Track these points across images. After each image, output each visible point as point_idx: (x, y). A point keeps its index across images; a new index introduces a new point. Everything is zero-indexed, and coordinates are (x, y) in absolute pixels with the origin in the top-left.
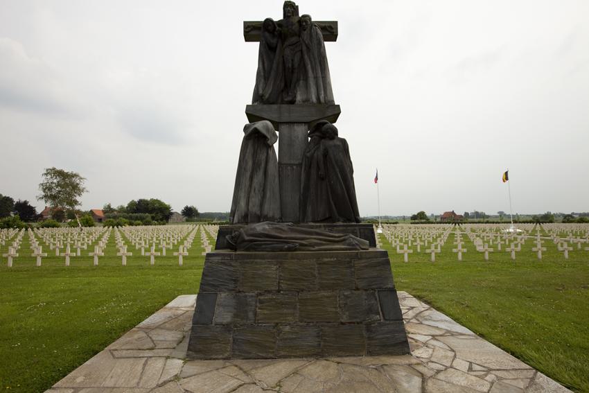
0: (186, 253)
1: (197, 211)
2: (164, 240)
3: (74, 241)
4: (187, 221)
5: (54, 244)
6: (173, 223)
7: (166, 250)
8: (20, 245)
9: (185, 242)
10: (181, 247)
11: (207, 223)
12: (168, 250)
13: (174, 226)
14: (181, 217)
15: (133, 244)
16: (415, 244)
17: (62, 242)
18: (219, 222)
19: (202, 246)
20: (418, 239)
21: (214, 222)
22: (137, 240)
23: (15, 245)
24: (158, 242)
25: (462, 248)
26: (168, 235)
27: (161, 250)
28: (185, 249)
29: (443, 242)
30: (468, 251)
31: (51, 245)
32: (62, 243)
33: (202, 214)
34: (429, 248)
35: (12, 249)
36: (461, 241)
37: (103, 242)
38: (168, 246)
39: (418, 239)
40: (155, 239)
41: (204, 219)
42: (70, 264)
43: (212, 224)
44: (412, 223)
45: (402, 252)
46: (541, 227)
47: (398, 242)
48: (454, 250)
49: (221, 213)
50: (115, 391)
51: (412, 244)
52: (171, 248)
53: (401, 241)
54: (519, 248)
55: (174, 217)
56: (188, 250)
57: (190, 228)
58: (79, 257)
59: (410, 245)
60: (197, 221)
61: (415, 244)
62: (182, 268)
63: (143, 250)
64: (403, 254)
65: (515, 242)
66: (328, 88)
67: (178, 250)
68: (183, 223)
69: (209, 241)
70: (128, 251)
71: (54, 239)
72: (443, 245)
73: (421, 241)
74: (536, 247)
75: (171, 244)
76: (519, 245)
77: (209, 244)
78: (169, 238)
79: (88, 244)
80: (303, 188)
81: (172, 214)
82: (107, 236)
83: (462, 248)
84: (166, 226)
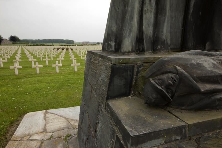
0: (63, 59)
1: (18, 38)
2: (51, 53)
3: (49, 53)
4: (13, 44)
5: (36, 53)
6: (4, 45)
8: (20, 55)
9: (62, 53)
10: (60, 56)
11: (25, 45)
12: (54, 57)
13: (5, 47)
14: (9, 41)
16: (44, 60)
17: (43, 53)
18: (33, 44)
19: (70, 55)
20: (47, 57)
21: (30, 44)
23: (19, 56)
24: (48, 54)
26: (2, 52)
27: (50, 58)
28: (62, 57)
30: (70, 65)
32: (43, 55)
33: (22, 40)
35: (18, 58)
37: (19, 55)
38: (54, 56)
39: (47, 57)
40: (46, 53)
41: (24, 43)
43: (29, 45)
44: (60, 45)
46: (22, 47)
47: (81, 54)
49: (32, 40)
52: (55, 56)
53: (83, 54)
55: (4, 41)
56: (63, 57)
57: (14, 47)
58: (52, 61)
59: (84, 53)
60: (19, 44)
61: (44, 60)
62: (18, 78)
65: (53, 54)
68: (11, 45)
69: (73, 53)
71: (34, 51)
73: (49, 58)
75: (55, 55)
77: (73, 54)
78: (4, 54)
79: (56, 55)
80: (194, 6)
81: (3, 40)
82: (20, 52)
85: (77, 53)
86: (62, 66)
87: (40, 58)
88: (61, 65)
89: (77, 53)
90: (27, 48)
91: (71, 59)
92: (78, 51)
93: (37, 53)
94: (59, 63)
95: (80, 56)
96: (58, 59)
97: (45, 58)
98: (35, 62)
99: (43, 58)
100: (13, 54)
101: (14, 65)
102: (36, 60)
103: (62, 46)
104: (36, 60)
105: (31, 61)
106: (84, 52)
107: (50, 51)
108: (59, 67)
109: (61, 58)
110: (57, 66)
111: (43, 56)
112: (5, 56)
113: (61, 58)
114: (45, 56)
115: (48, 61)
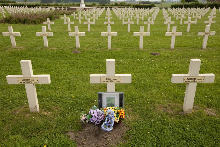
5: (122, 16)
7: (139, 21)
15: (174, 16)
22: (123, 16)
25: (111, 21)
28: (152, 20)
29: (97, 17)
31: (120, 17)
34: (147, 20)
36: (110, 16)
42: (54, 35)
45: (126, 23)
46: (113, 14)
48: (105, 23)
50: (91, 4)
54: (153, 22)
63: (123, 20)
64: (127, 25)
65: (92, 18)
66: (157, 2)
67: (147, 20)
70: (172, 20)
72: (156, 18)
74: (107, 21)
76: (94, 20)
83: (111, 21)
84: (165, 10)
85: (119, 18)
86: (149, 35)
87: (179, 20)
88: (148, 33)
89: (121, 18)
90: (116, 11)
91: (165, 23)
92: (121, 13)
93: (124, 15)
94: (146, 30)
95: (122, 20)
96: (145, 23)
97: (187, 20)
98: (171, 25)
99: (184, 20)
100: (99, 16)
101: (42, 31)
102: (73, 23)
103: (36, 8)
104: (173, 22)
105: (67, 25)
106: (179, 16)
107: (87, 13)
108: (145, 37)
109: (151, 21)
110: (142, 34)
111: (185, 17)
112: (79, 17)
113: (151, 21)
114: (187, 16)
115: (131, 25)
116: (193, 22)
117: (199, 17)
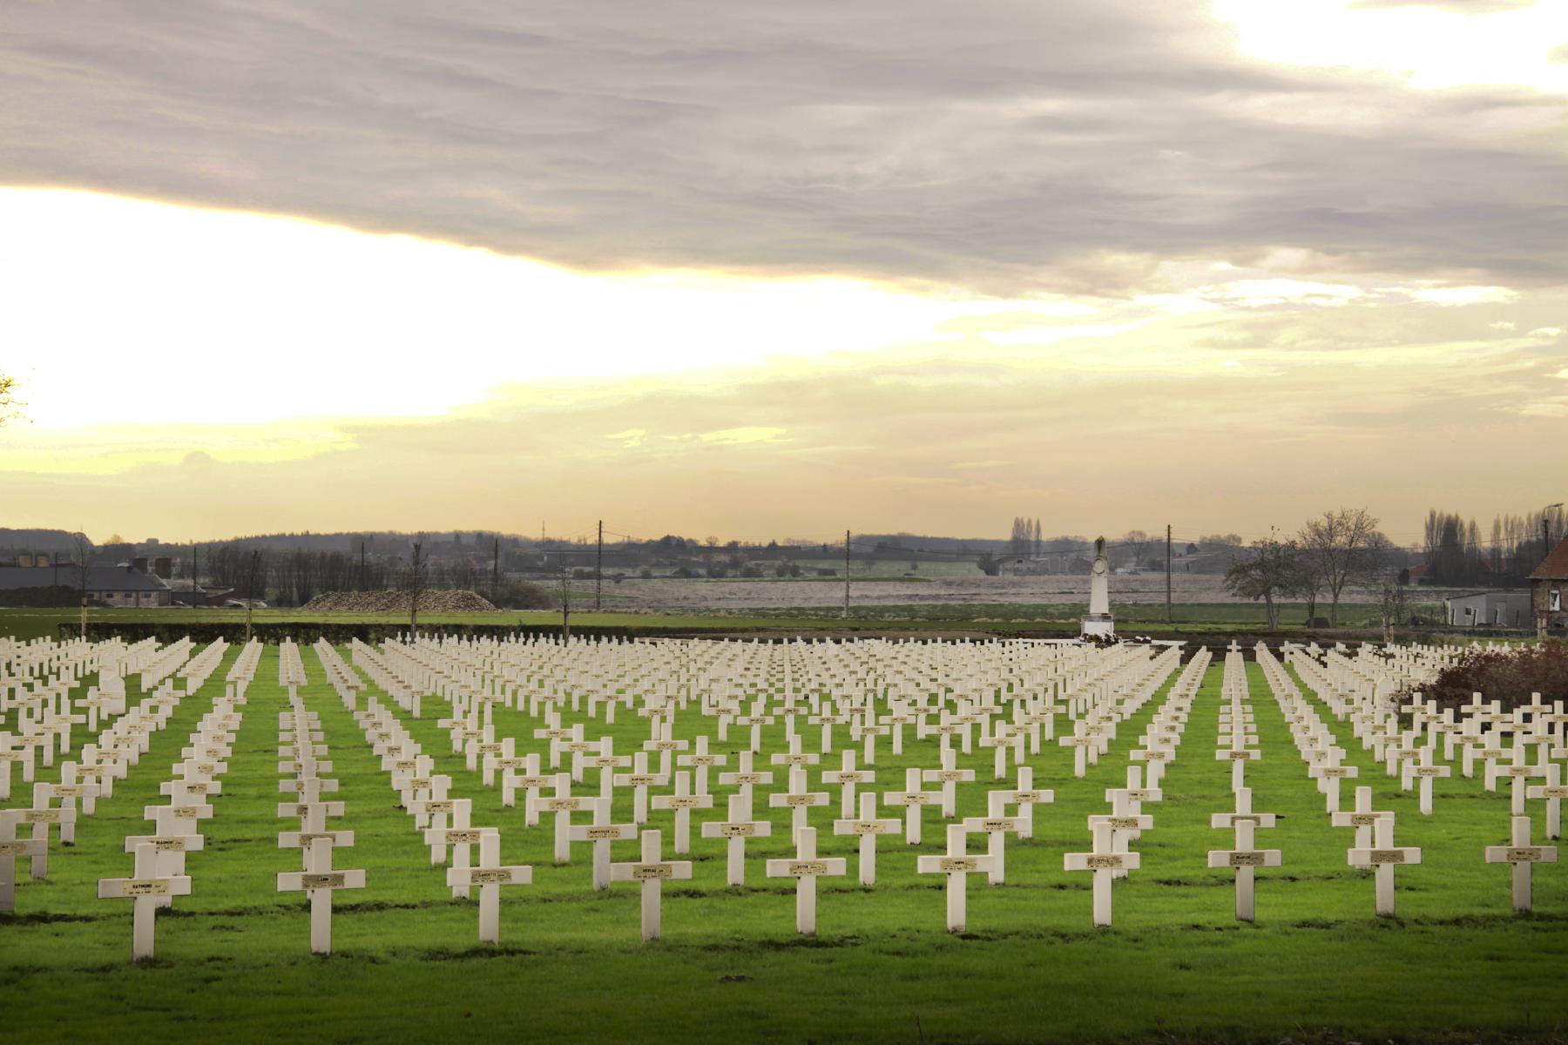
16: (710, 829)
24: (763, 828)
51: (695, 831)
106: (654, 790)
116: (892, 826)
117: (933, 798)
